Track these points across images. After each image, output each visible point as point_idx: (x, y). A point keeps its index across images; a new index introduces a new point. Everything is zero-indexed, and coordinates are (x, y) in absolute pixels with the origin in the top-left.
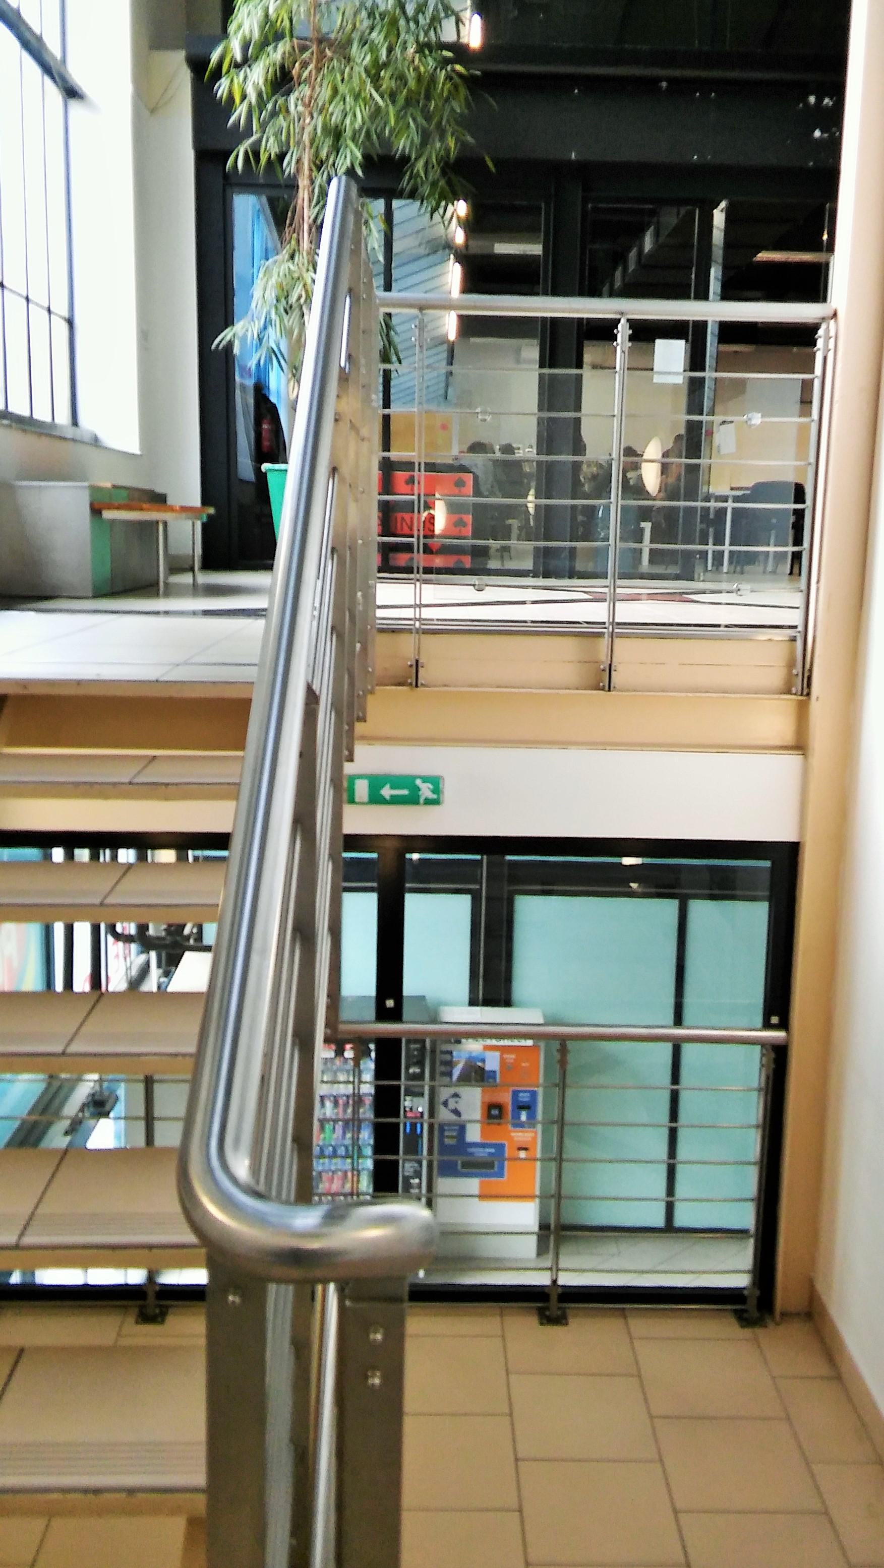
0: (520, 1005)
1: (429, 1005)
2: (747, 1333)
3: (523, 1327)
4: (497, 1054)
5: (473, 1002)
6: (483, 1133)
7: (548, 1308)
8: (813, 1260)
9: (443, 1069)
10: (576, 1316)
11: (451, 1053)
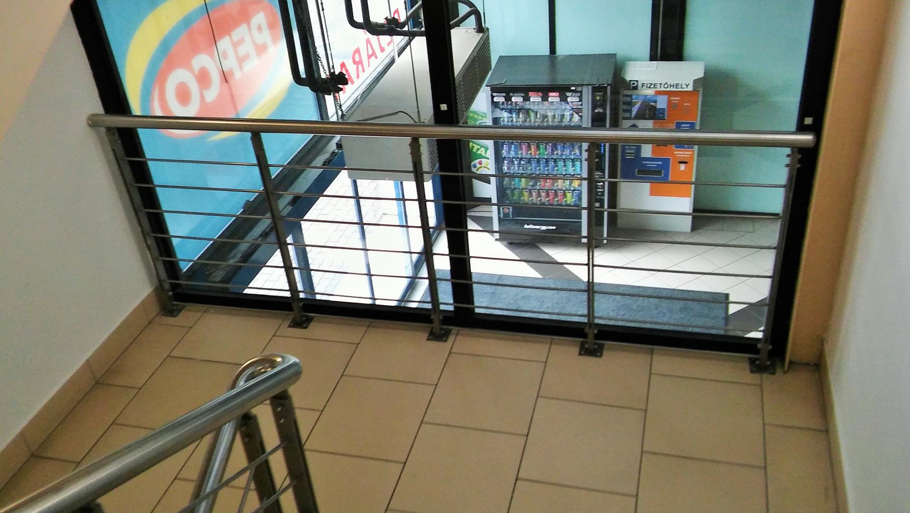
0: (690, 59)
1: (618, 60)
2: (755, 378)
3: (565, 353)
4: (665, 97)
5: (653, 58)
6: (653, 152)
7: (586, 343)
8: (821, 342)
9: (625, 107)
10: (610, 349)
11: (631, 96)
